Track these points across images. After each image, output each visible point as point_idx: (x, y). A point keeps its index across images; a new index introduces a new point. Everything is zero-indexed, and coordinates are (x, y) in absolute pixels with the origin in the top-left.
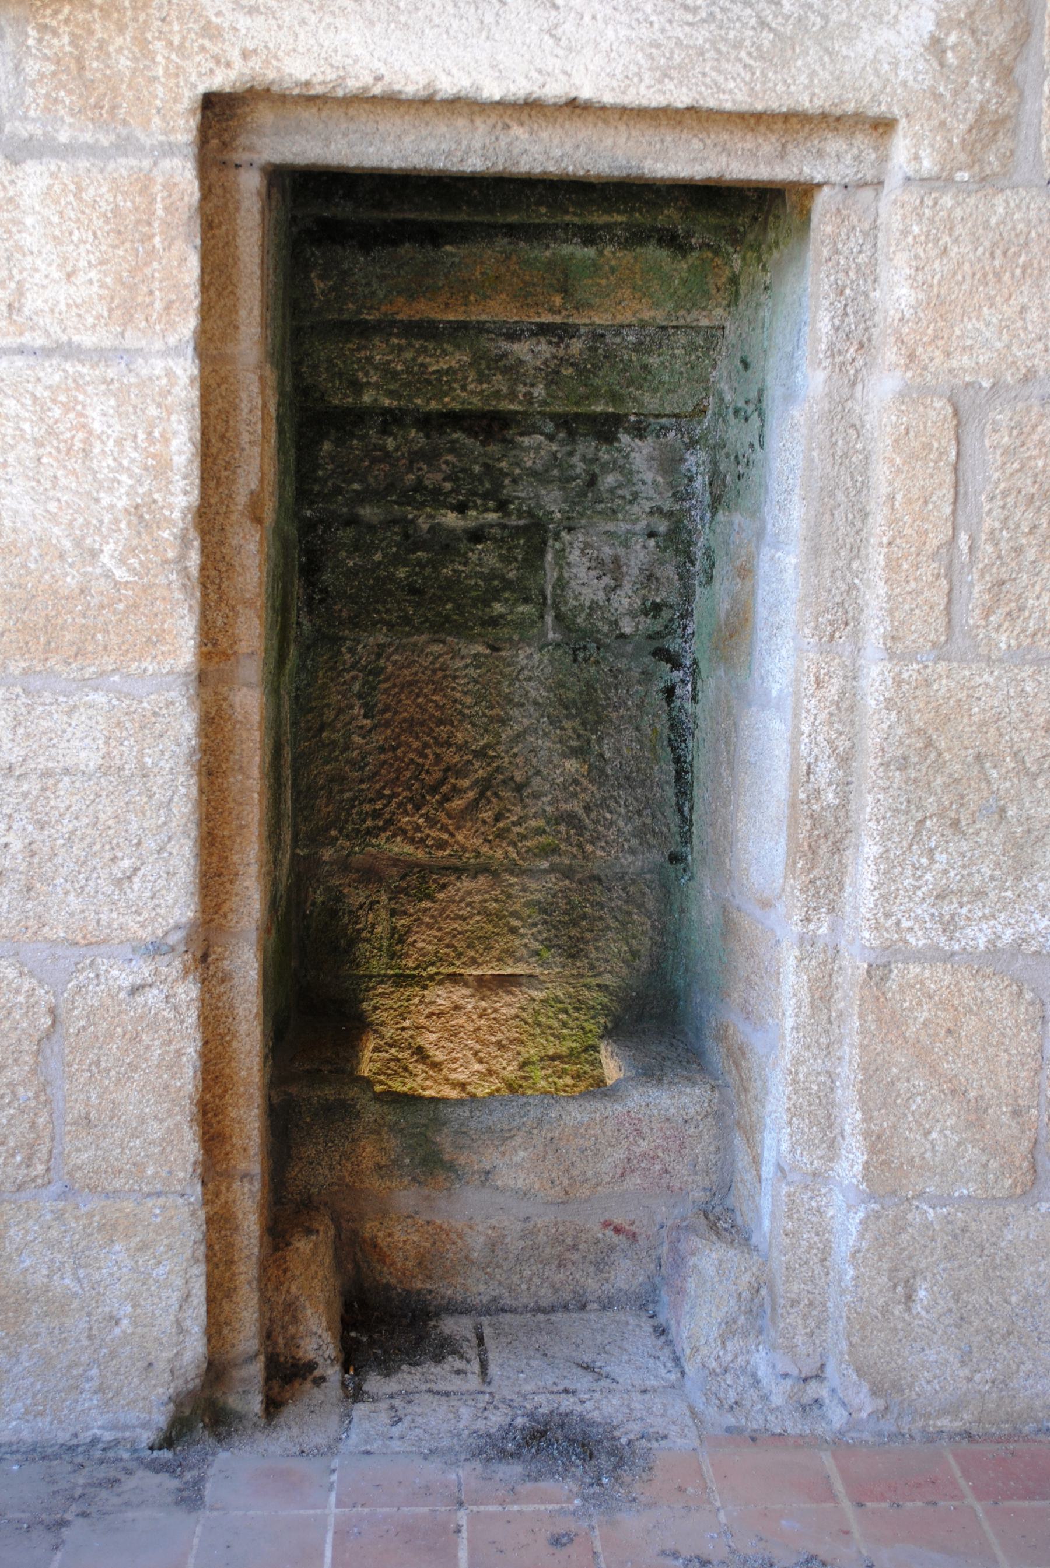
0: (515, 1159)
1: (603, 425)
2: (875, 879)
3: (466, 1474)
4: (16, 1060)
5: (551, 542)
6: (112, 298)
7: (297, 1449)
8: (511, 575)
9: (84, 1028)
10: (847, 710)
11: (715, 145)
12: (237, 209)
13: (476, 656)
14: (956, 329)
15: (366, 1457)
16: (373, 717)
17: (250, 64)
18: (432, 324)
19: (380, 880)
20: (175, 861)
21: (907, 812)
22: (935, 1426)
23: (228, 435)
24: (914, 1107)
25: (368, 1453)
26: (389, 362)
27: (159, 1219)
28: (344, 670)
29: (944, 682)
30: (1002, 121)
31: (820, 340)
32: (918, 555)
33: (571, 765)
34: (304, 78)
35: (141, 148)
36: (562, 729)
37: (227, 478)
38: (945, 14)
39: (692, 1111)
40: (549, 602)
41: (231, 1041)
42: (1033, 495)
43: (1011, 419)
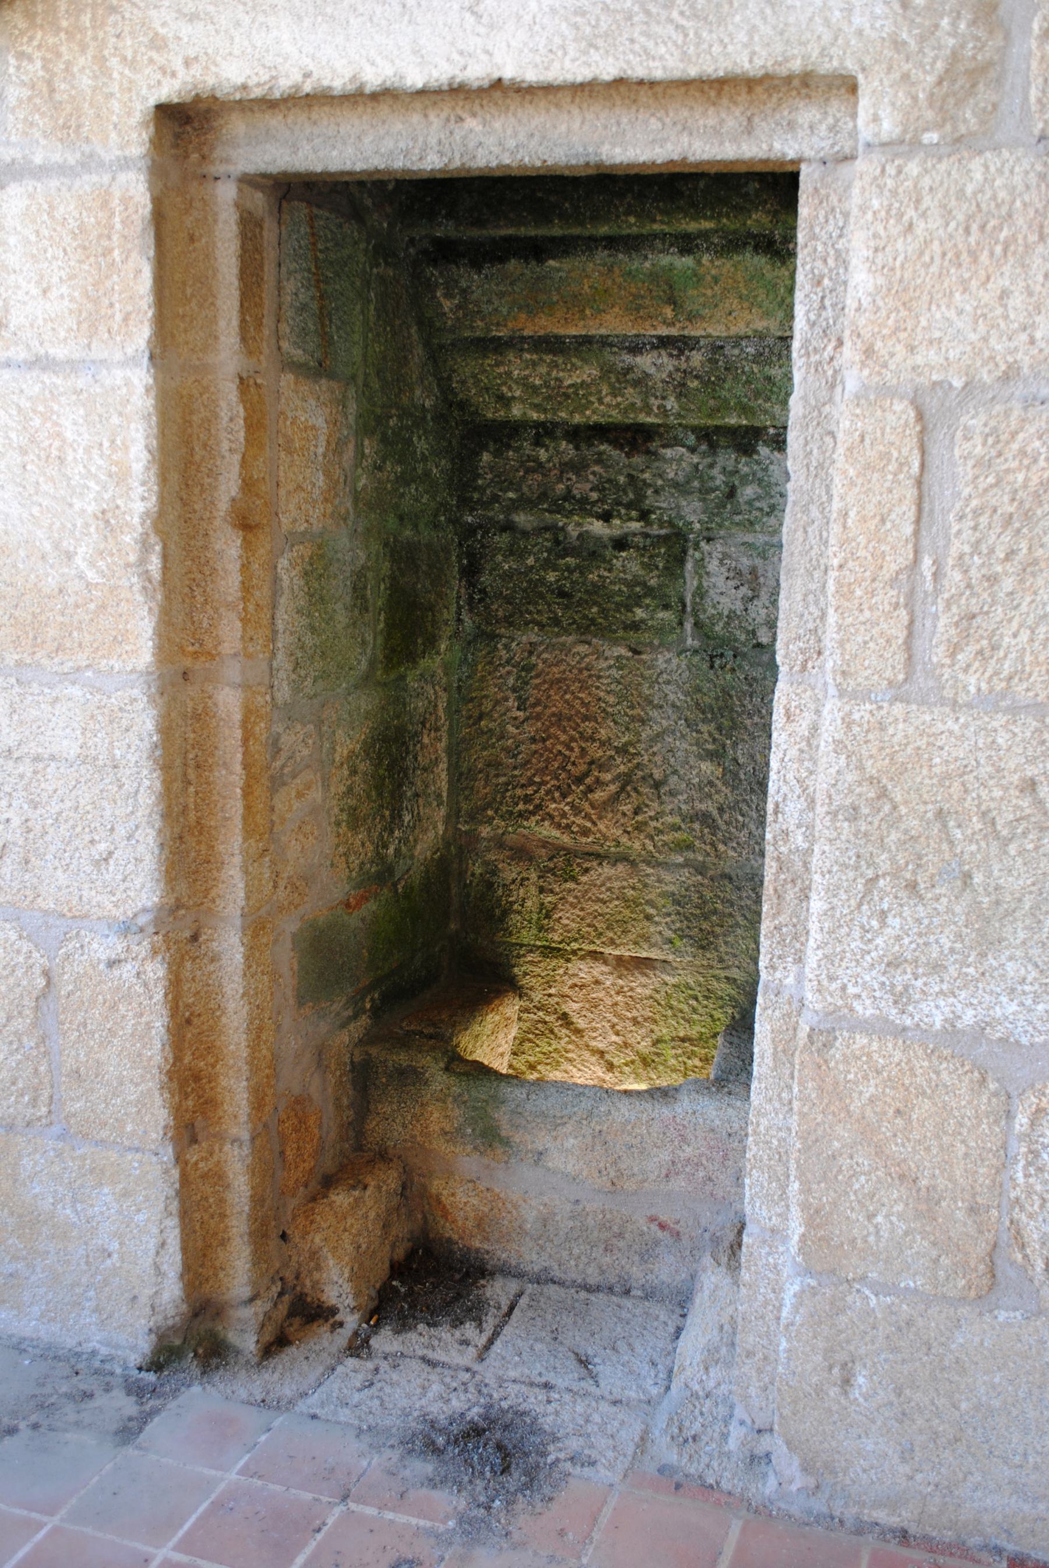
0: (566, 1145)
1: (743, 438)
2: (819, 937)
3: (373, 1463)
4: (20, 1013)
5: (691, 552)
6: (80, 311)
8: (653, 582)
11: (675, 123)
12: (215, 221)
13: (618, 658)
14: (922, 319)
16: (525, 709)
17: (192, 72)
20: (141, 848)
21: (857, 868)
22: (869, 1515)
23: (210, 443)
24: (857, 1186)
26: (526, 377)
29: (901, 726)
30: (984, 68)
32: (874, 580)
33: (707, 767)
34: (240, 81)
35: (101, 164)
36: (698, 732)
37: (210, 485)
40: (689, 609)
42: (1011, 515)
43: (985, 425)
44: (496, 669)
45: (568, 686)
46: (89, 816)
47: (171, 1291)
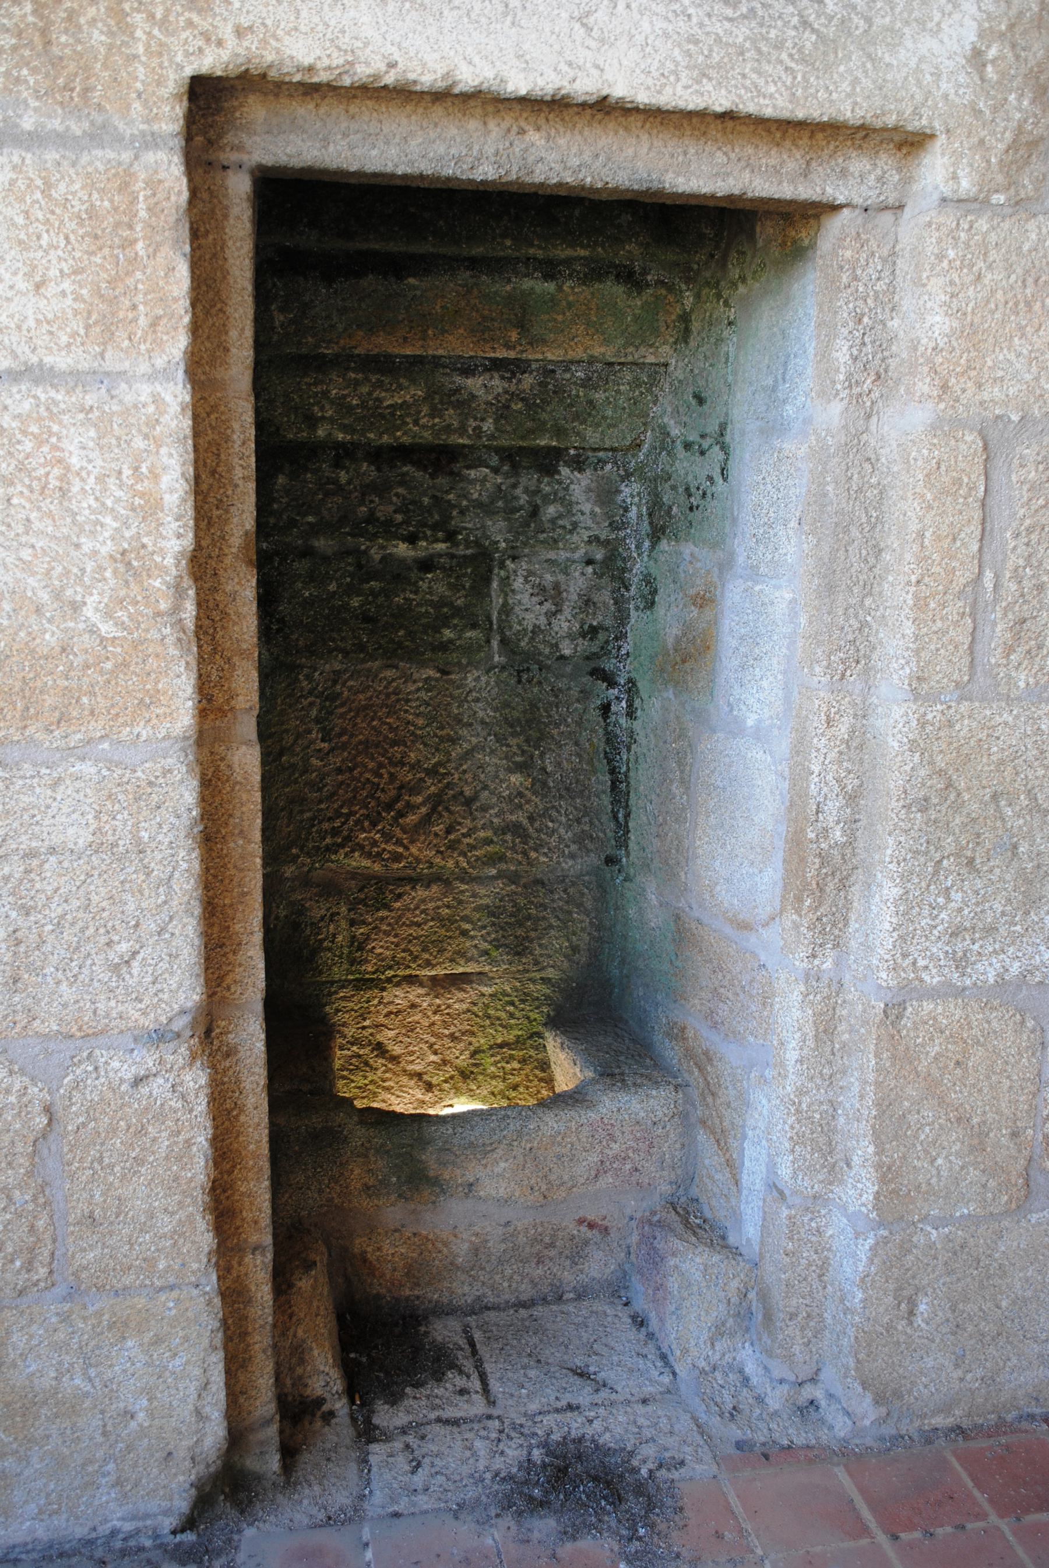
0: (496, 1170)
1: (545, 458)
2: (894, 920)
4: (9, 1164)
5: (496, 571)
6: (89, 313)
7: (322, 1516)
9: (84, 1125)
10: (856, 748)
12: (226, 216)
13: (428, 679)
15: (396, 1521)
16: (330, 740)
17: (246, 44)
18: (389, 358)
19: (340, 893)
20: (178, 942)
21: (926, 853)
23: (219, 469)
24: (923, 1137)
25: (396, 1515)
26: (345, 397)
27: (173, 1312)
28: (301, 696)
29: (966, 722)
31: (838, 371)
33: (515, 779)
34: (307, 61)
35: (119, 139)
36: (508, 745)
37: (219, 517)
38: (987, 25)
39: (659, 1113)
41: (238, 1115)
44: (297, 702)
45: (375, 713)
46: (105, 914)
47: (214, 1433)
